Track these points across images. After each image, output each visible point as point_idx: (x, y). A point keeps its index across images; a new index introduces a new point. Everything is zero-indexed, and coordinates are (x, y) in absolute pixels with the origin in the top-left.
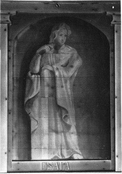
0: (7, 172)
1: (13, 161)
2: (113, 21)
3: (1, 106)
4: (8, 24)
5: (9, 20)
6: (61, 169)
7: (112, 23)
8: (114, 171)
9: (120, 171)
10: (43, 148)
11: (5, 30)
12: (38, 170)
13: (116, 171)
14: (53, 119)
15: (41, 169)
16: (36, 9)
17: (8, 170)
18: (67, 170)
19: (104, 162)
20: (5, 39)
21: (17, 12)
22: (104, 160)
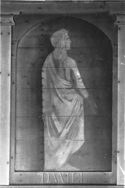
0: (9, 184)
1: (16, 171)
2: (116, 21)
3: (2, 92)
4: (12, 27)
5: (13, 22)
6: (68, 181)
7: (115, 23)
8: (116, 185)
9: (114, 183)
10: (73, 139)
11: (9, 75)
12: (38, 183)
13: (117, 184)
14: (54, 130)
15: (73, 182)
16: (12, 158)
17: (11, 183)
18: (54, 183)
19: (105, 174)
20: (9, 51)
21: (21, 13)
22: (105, 173)
